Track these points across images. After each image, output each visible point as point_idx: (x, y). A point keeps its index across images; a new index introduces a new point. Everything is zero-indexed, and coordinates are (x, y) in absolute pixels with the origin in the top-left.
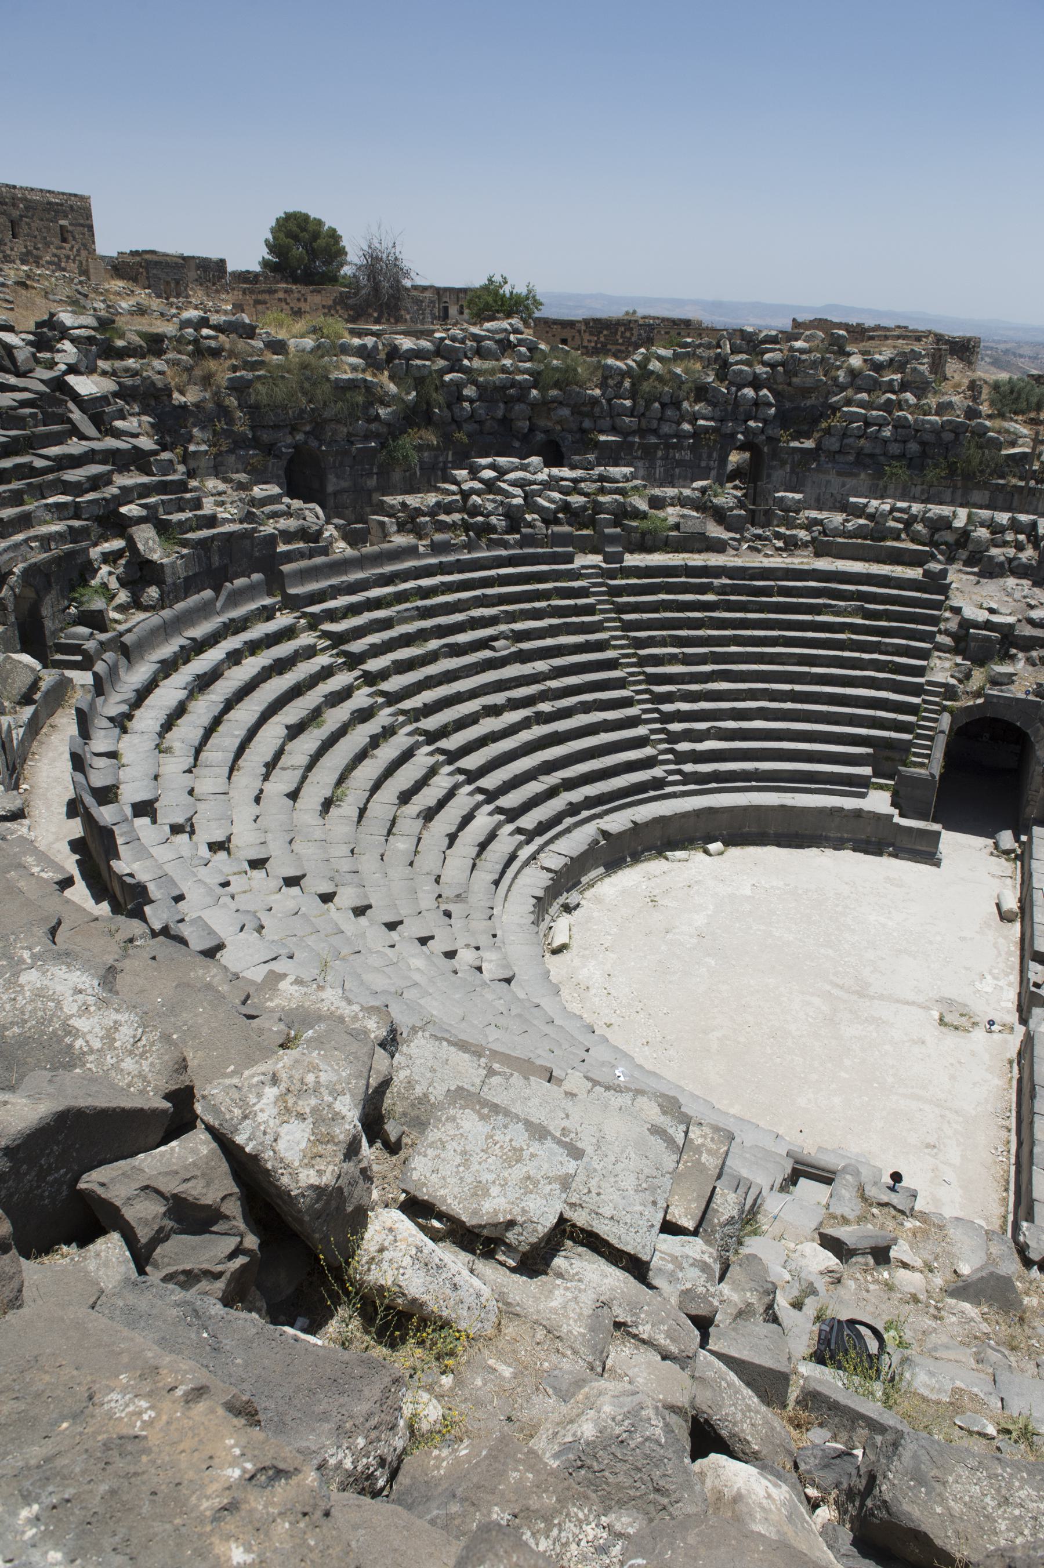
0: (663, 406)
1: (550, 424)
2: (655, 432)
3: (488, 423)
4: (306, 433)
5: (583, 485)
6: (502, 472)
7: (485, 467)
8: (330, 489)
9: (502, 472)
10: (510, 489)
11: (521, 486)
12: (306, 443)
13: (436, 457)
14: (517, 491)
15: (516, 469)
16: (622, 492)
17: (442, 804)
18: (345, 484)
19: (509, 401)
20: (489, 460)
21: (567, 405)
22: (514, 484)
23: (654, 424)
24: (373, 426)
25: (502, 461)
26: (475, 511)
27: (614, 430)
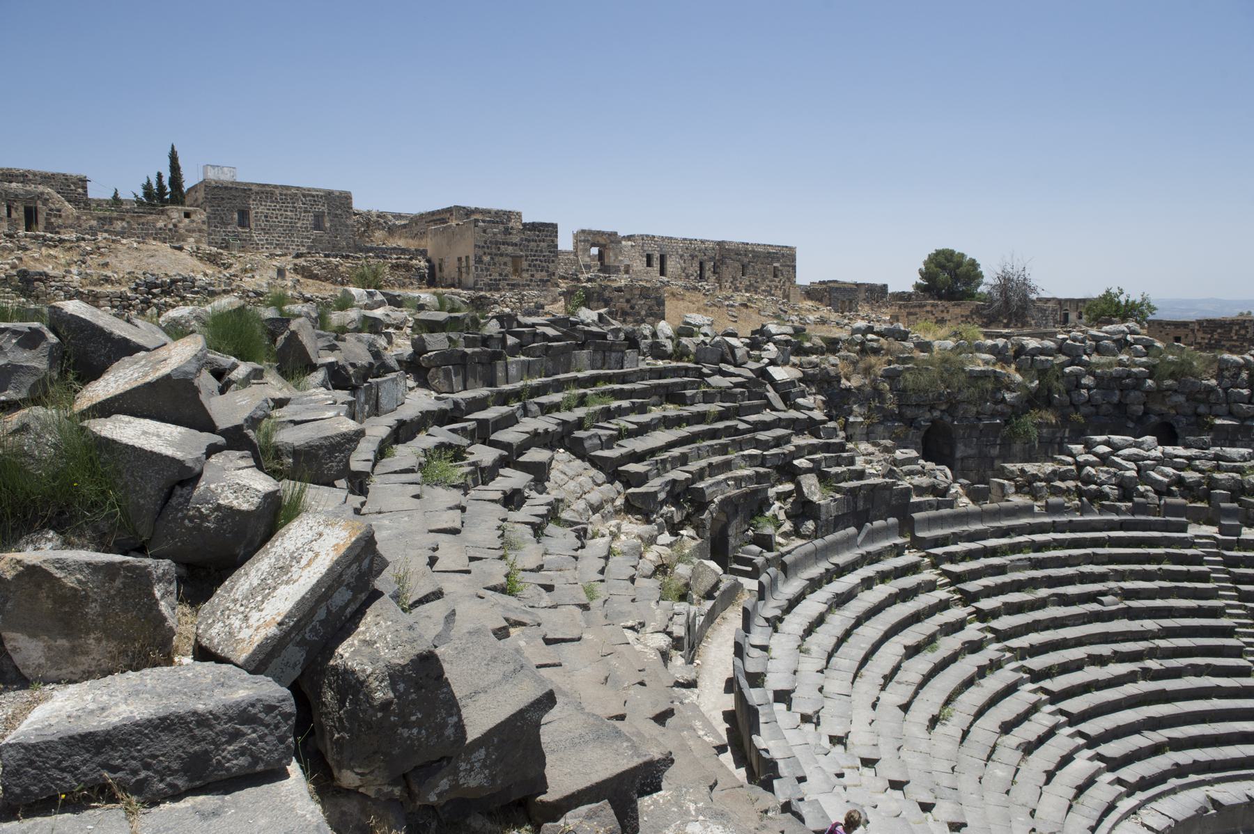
1: (1164, 409)
3: (1104, 407)
5: (1197, 462)
6: (1116, 448)
7: (1100, 443)
8: (958, 455)
9: (1116, 448)
10: (1124, 463)
11: (1135, 461)
12: (941, 418)
13: (1054, 433)
14: (1131, 465)
15: (1130, 446)
16: (1239, 470)
17: (1041, 740)
18: (970, 452)
19: (1124, 389)
20: (1104, 437)
21: (1182, 393)
22: (1127, 458)
25: (1116, 438)
26: (1089, 480)
27: (1230, 415)
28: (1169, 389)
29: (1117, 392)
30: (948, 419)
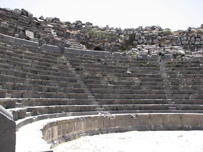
0: (195, 38)
2: (194, 44)
21: (169, 40)
23: (193, 42)
28: (164, 39)
29: (151, 40)
30: (102, 46)
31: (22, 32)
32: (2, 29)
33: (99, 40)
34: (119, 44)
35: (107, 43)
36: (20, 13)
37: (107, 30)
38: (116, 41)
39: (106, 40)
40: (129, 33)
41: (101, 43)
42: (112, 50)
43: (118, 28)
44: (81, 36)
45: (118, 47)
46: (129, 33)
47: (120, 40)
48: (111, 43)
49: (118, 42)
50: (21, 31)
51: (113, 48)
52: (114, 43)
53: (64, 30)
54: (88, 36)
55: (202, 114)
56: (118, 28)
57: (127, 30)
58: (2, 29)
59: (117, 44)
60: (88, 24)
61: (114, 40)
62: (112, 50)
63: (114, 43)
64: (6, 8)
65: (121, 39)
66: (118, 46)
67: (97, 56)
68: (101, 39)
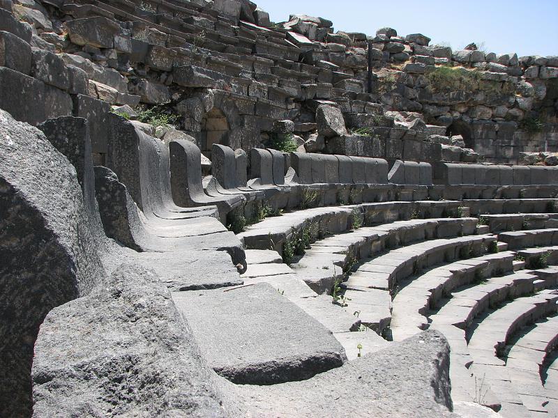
4: (460, 113)
12: (461, 119)
24: (514, 111)
30: (467, 119)
31: (293, 105)
32: (255, 110)
33: (460, 100)
34: (518, 114)
35: (482, 108)
36: (235, 14)
37: (478, 64)
38: (510, 103)
39: (480, 97)
40: (545, 75)
41: (462, 110)
42: (497, 132)
43: (511, 57)
44: (407, 86)
45: (514, 124)
46: (545, 75)
47: (519, 98)
48: (491, 108)
49: (516, 104)
50: (291, 104)
51: (502, 127)
52: (503, 110)
53: (359, 69)
54: (430, 88)
55: (555, 248)
56: (511, 57)
57: (541, 63)
58: (255, 110)
59: (511, 111)
60: (418, 40)
61: (503, 98)
62: (497, 132)
63: (503, 110)
64: (382, 28)
65: (527, 96)
66: (514, 118)
67: (538, 186)
68: (467, 95)
